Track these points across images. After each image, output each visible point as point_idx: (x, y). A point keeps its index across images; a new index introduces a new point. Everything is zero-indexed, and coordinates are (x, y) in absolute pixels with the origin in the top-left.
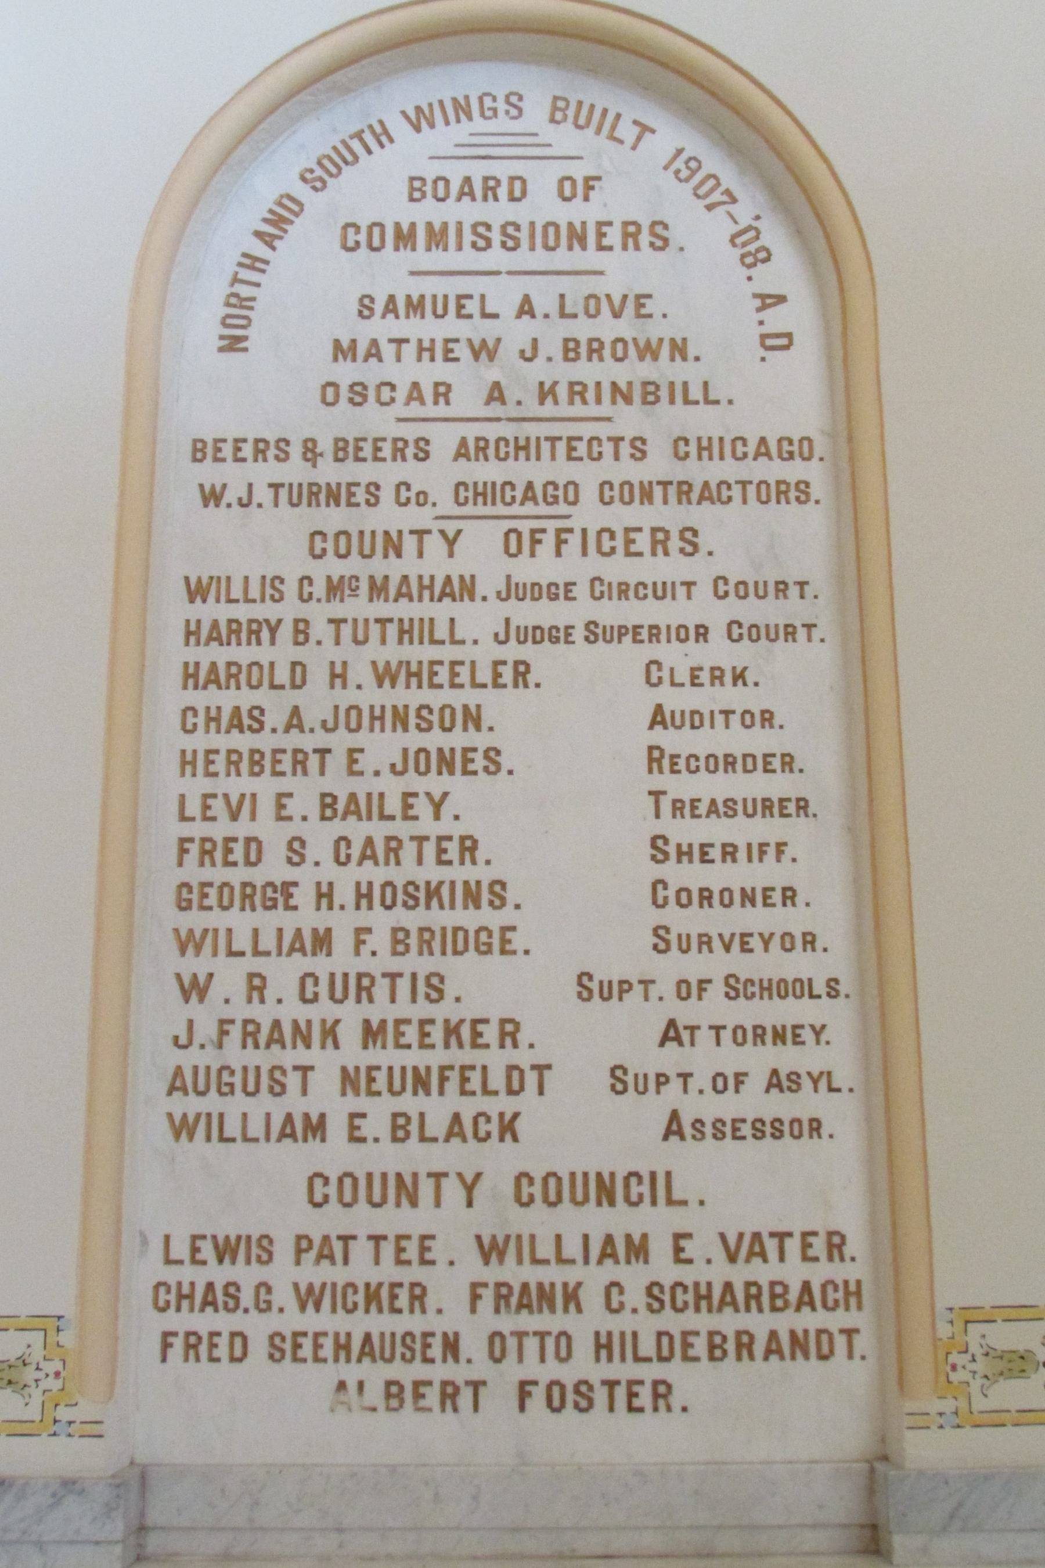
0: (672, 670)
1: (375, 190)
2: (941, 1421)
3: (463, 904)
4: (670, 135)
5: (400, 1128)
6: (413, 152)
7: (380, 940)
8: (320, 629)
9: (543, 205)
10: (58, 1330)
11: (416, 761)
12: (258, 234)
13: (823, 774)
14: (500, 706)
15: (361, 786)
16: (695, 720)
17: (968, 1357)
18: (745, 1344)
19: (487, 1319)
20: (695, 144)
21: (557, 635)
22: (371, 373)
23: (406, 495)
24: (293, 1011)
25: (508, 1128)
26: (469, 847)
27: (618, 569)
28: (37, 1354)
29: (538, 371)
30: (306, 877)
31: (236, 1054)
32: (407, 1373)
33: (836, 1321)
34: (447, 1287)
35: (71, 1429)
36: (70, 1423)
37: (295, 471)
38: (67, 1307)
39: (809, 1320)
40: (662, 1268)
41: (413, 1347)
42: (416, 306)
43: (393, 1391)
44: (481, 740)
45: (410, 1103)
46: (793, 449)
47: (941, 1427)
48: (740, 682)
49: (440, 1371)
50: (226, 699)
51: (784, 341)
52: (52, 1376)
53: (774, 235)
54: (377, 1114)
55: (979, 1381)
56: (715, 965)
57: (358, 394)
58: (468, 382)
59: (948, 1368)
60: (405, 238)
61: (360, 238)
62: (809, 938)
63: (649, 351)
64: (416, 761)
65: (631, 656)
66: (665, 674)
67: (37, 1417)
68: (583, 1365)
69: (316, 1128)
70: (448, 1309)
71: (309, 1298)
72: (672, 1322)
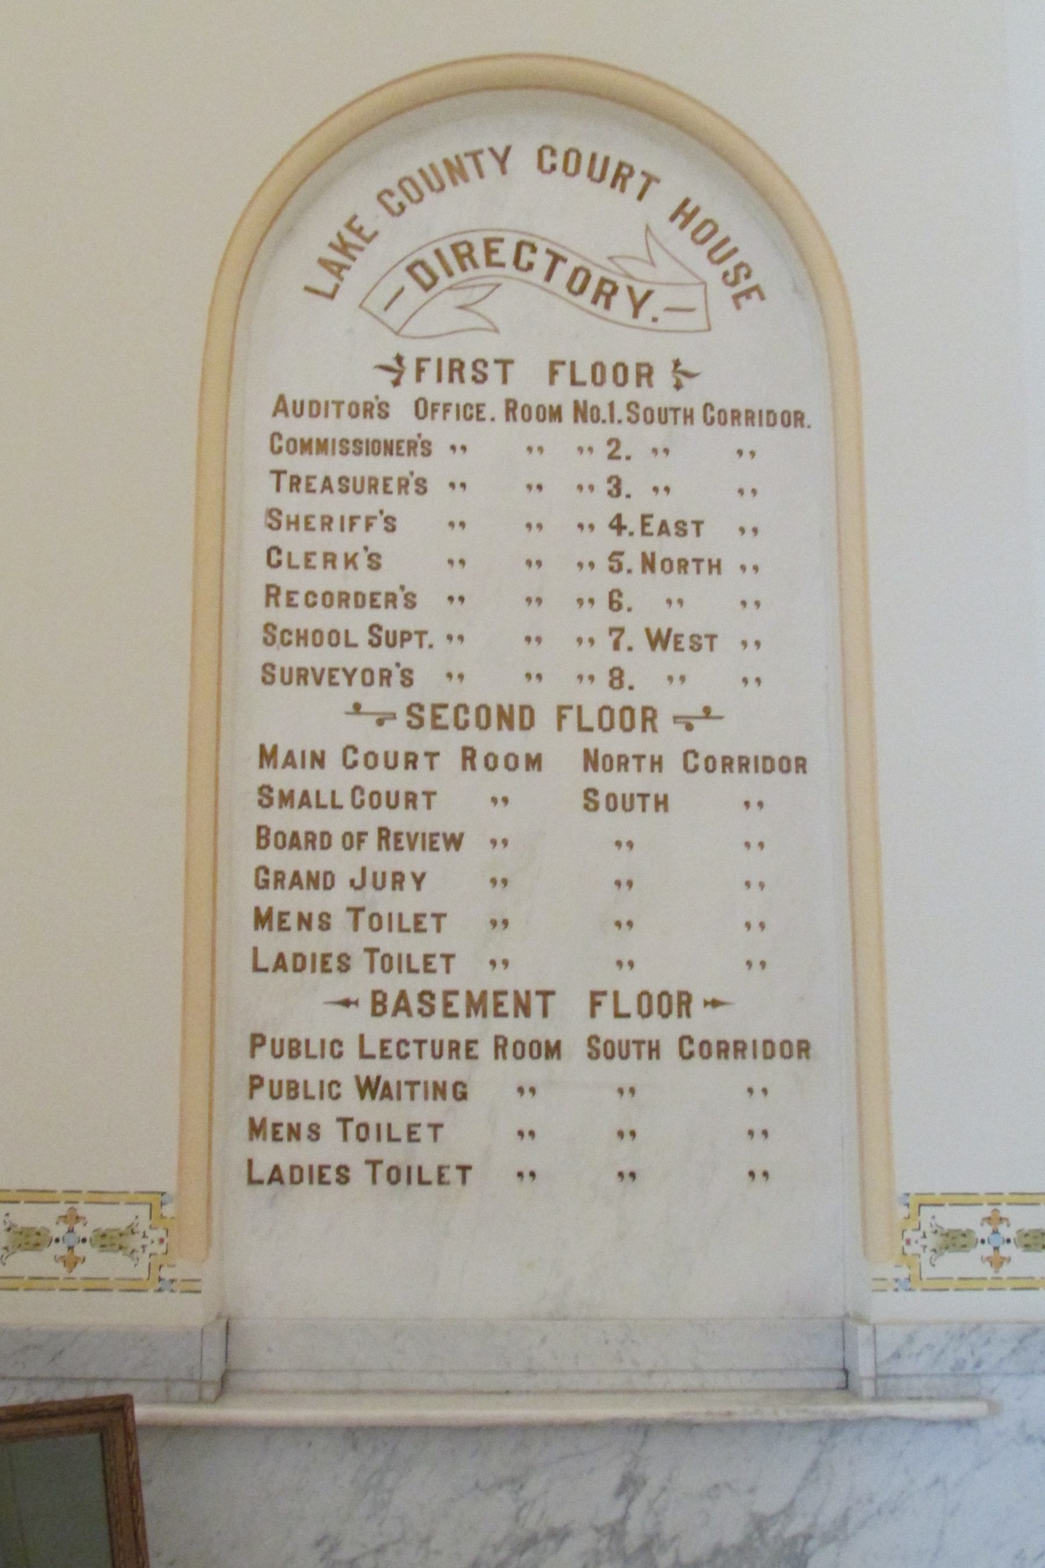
0: (290, 554)
2: (897, 1285)
10: (162, 1204)
12: (323, 262)
17: (920, 1234)
28: (144, 1224)
35: (174, 1286)
36: (172, 1281)
38: (169, 1185)
47: (896, 1290)
48: (351, 566)
52: (157, 1242)
55: (928, 1254)
59: (904, 1243)
62: (411, 758)
66: (284, 557)
67: (145, 1276)
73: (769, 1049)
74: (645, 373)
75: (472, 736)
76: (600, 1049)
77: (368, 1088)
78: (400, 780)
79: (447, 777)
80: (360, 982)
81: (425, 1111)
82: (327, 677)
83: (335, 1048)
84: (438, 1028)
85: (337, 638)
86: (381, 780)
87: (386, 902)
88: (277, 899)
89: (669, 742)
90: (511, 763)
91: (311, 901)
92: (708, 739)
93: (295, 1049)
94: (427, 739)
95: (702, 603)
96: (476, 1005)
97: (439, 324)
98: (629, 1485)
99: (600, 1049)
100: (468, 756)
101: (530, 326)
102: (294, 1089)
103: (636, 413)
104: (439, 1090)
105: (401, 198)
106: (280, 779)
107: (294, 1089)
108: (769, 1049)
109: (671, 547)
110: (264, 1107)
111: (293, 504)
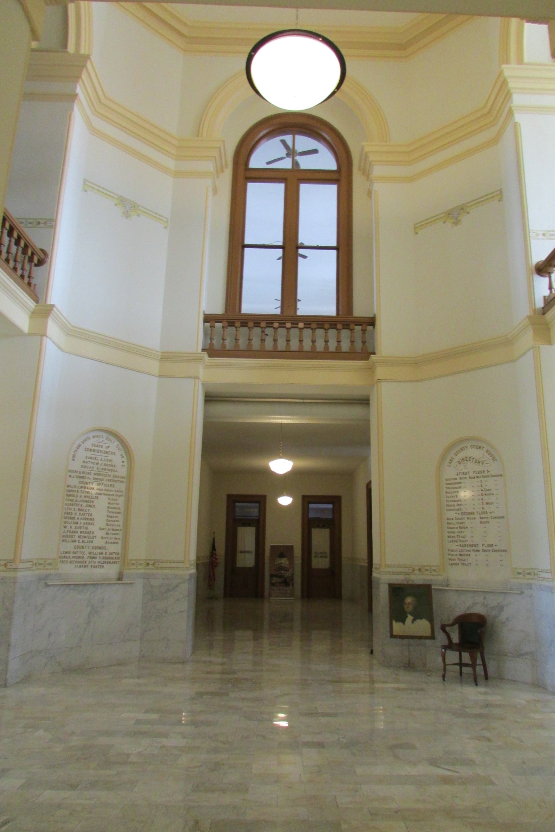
1: (88, 445)
3: (90, 520)
4: (117, 443)
5: (83, 542)
6: (93, 441)
7: (83, 523)
8: (79, 492)
9: (104, 449)
11: (87, 506)
13: (122, 510)
14: (96, 501)
15: (82, 508)
16: (112, 504)
18: (110, 562)
19: (89, 560)
20: (119, 444)
21: (101, 494)
22: (86, 465)
23: (89, 478)
24: (74, 530)
25: (92, 542)
26: (91, 515)
27: (108, 488)
29: (102, 467)
30: (76, 517)
31: (69, 534)
32: (81, 564)
33: (118, 560)
34: (86, 556)
37: (78, 474)
39: (116, 560)
40: (104, 555)
41: (82, 562)
42: (91, 458)
43: (80, 566)
44: (93, 504)
45: (83, 539)
46: (123, 478)
49: (84, 564)
50: (70, 498)
51: (123, 466)
53: (124, 455)
54: (81, 540)
56: (111, 527)
57: (85, 467)
58: (96, 467)
60: (91, 450)
61: (87, 450)
63: (112, 466)
64: (87, 506)
65: (107, 497)
68: (97, 564)
69: (75, 541)
70: (86, 559)
71: (73, 557)
72: (105, 560)
73: (502, 551)
74: (484, 472)
75: (468, 516)
76: (484, 551)
77: (460, 555)
78: (461, 521)
79: (466, 520)
80: (458, 543)
81: (466, 557)
82: (453, 510)
83: (456, 551)
84: (467, 548)
85: (453, 505)
86: (459, 521)
87: (460, 534)
88: (449, 534)
89: (489, 515)
90: (472, 519)
91: (453, 535)
92: (493, 515)
93: (453, 551)
94: (463, 516)
95: (492, 499)
96: (470, 546)
97: (461, 468)
98: (484, 598)
99: (484, 551)
100: (468, 518)
101: (471, 467)
102: (453, 555)
103: (484, 477)
104: (467, 555)
105: (456, 454)
106: (449, 521)
107: (453, 555)
108: (502, 551)
109: (488, 492)
110: (450, 557)
111: (448, 491)
